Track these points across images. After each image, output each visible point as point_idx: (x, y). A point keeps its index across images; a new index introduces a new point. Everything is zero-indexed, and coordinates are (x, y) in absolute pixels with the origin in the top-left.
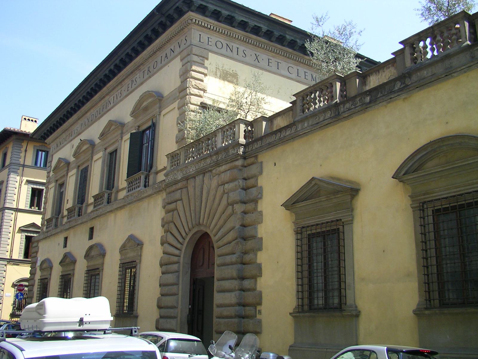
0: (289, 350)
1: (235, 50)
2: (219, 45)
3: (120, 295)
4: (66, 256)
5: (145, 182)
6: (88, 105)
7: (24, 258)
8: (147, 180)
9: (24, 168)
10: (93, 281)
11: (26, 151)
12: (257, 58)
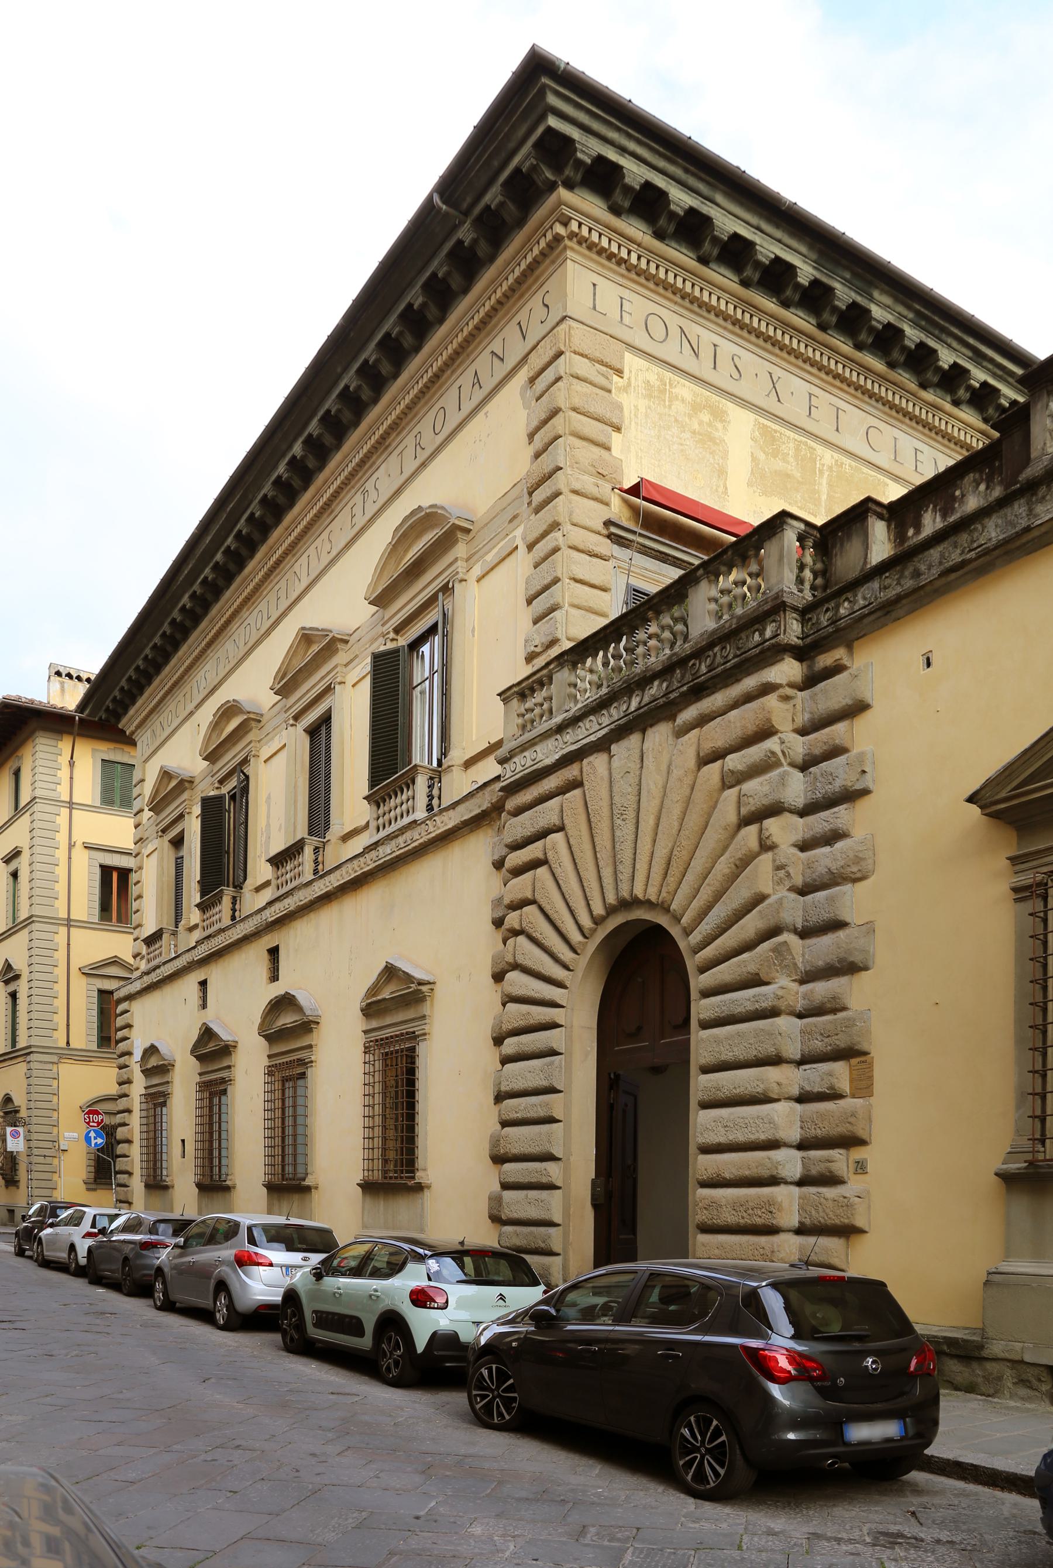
0: (987, 1283)
1: (706, 353)
2: (658, 331)
3: (373, 1128)
4: (207, 1033)
5: (431, 797)
6: (231, 597)
7: (98, 1047)
8: (435, 792)
9: (68, 800)
10: (289, 1093)
11: (72, 764)
12: (774, 387)
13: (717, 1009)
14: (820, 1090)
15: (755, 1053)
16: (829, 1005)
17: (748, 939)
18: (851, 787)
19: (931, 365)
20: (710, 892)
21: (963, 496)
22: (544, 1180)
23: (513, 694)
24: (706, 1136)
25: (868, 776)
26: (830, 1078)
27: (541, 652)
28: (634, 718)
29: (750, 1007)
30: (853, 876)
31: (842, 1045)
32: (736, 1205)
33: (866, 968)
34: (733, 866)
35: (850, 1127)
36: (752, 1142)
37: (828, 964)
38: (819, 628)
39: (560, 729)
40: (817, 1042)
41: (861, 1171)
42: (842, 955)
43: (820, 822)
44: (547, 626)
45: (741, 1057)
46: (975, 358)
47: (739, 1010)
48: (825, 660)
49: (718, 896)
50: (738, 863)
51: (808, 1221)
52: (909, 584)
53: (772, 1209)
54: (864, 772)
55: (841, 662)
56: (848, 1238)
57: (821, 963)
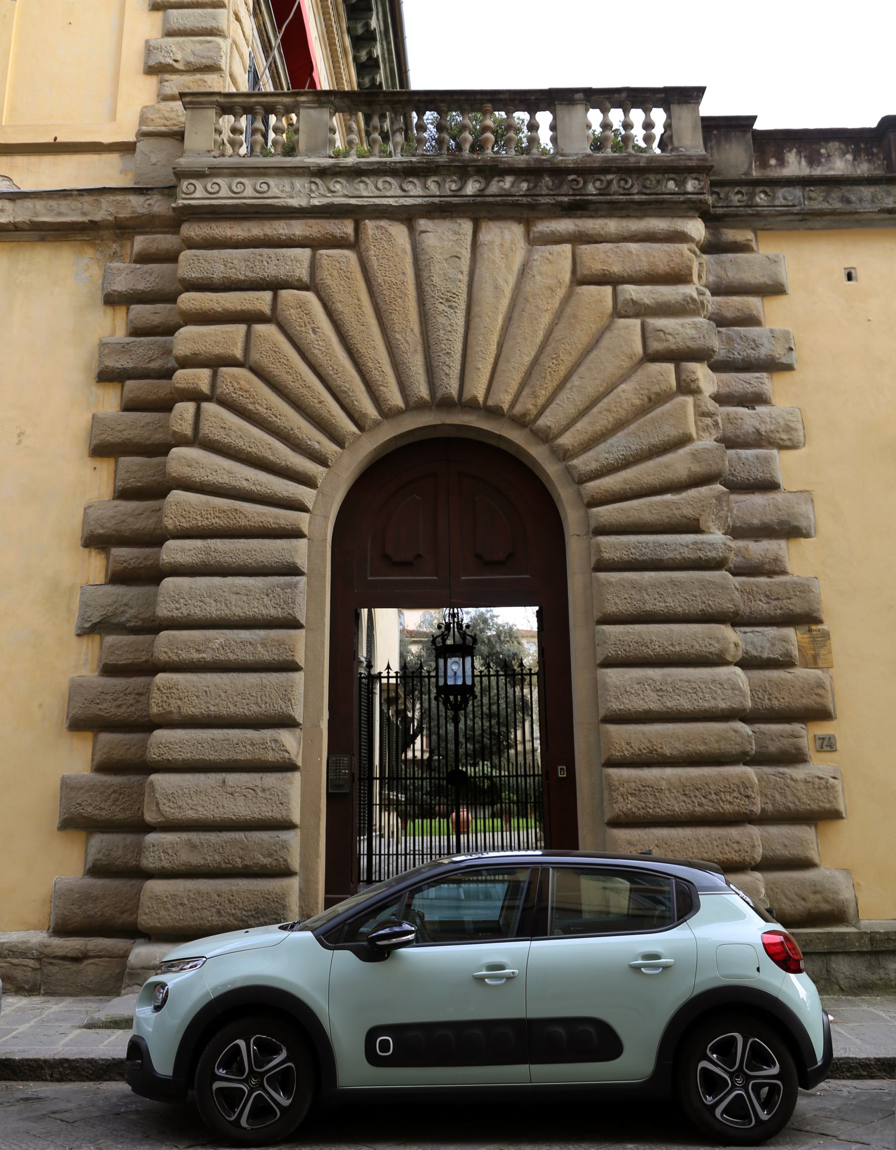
13: (633, 551)
14: (772, 656)
15: (702, 607)
16: (767, 567)
17: (676, 480)
18: (778, 359)
19: (364, 19)
20: (611, 419)
21: (829, 156)
22: (271, 757)
23: (212, 103)
24: (626, 701)
25: (794, 354)
26: (784, 644)
27: (182, 71)
28: (465, 204)
29: (687, 554)
30: (781, 442)
31: (798, 610)
32: (684, 789)
33: (807, 536)
34: (646, 399)
35: (819, 700)
36: (706, 710)
37: (765, 524)
38: (730, 204)
39: (322, 173)
40: (761, 604)
41: (829, 749)
42: (785, 518)
43: (740, 382)
44: (199, 47)
45: (680, 609)
46: (383, 33)
47: (671, 555)
48: (732, 235)
49: (619, 425)
50: (653, 396)
51: (769, 807)
52: (838, 205)
53: (750, 793)
54: (791, 349)
55: (750, 243)
56: (821, 824)
57: (756, 521)
